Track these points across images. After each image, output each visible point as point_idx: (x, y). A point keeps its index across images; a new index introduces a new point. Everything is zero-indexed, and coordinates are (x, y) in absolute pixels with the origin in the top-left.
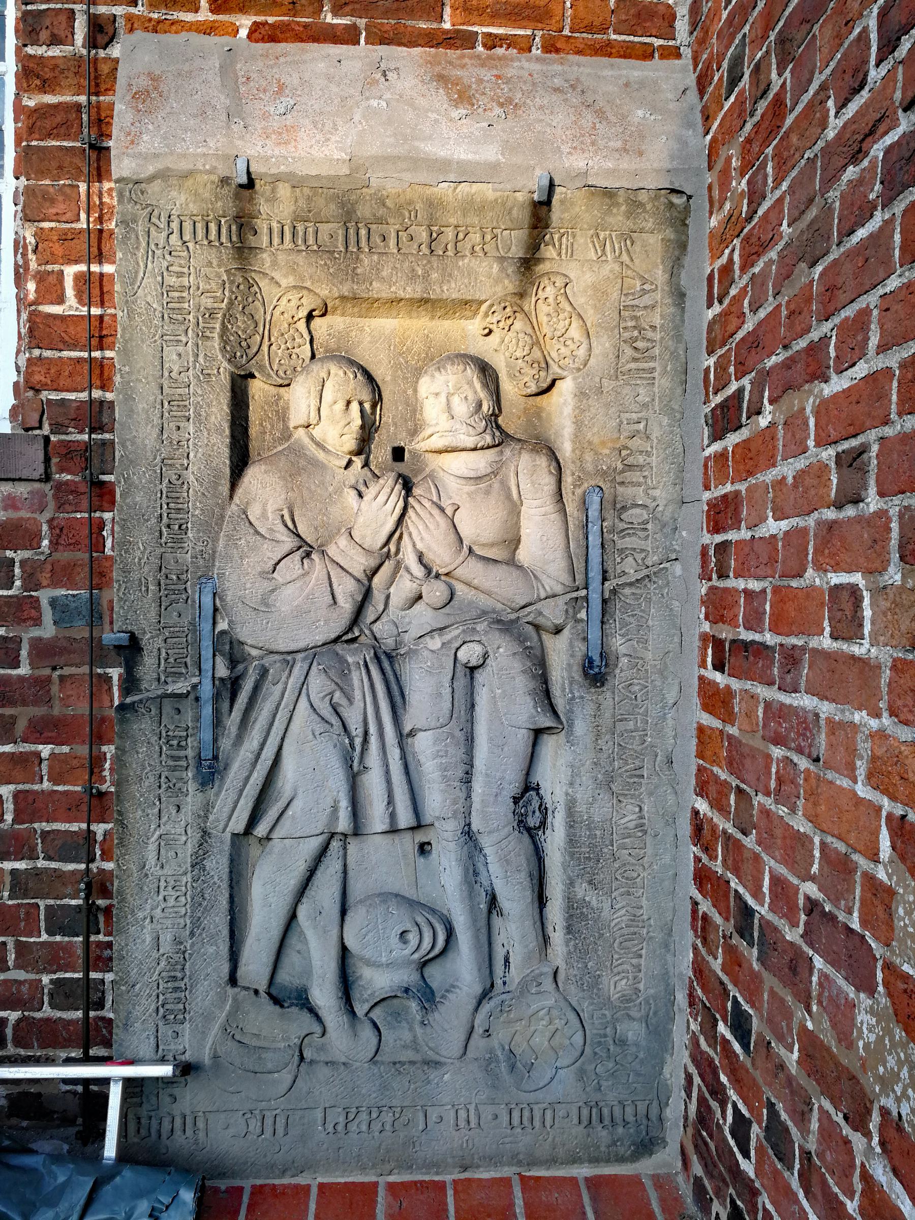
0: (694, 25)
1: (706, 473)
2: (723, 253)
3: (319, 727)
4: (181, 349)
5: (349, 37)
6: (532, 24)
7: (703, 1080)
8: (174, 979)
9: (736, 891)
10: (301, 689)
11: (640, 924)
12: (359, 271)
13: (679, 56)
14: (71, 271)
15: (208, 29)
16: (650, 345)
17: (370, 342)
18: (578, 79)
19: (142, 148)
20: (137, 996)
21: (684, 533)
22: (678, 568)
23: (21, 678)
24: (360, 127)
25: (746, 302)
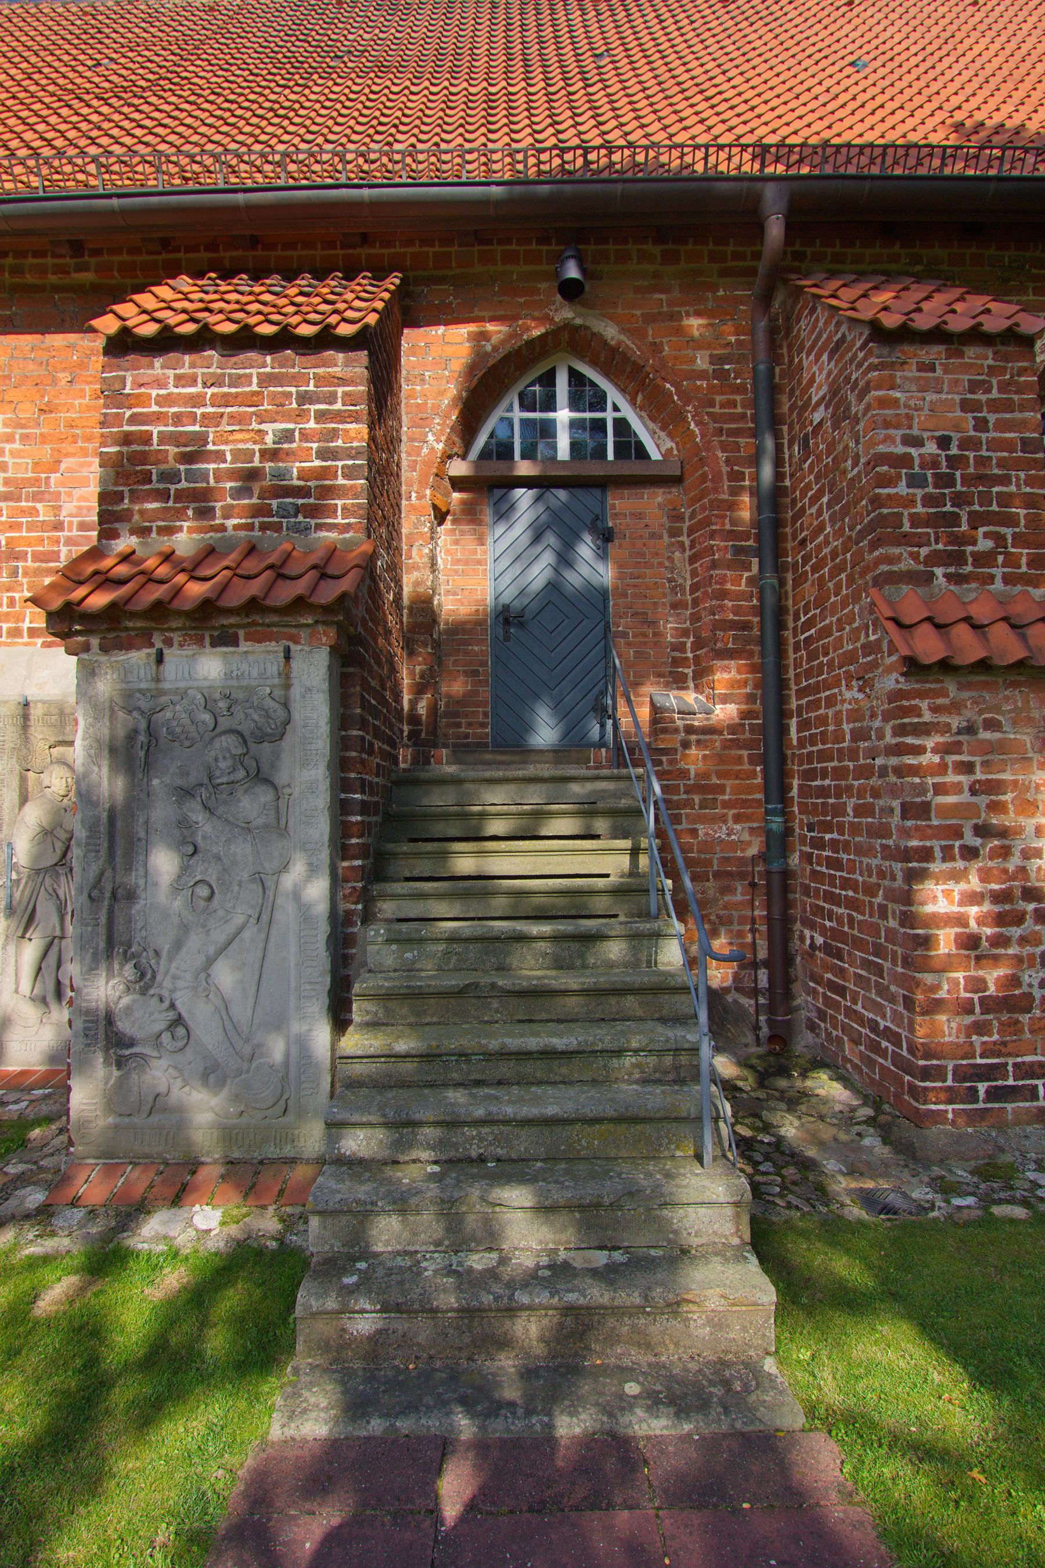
15: (26, 644)
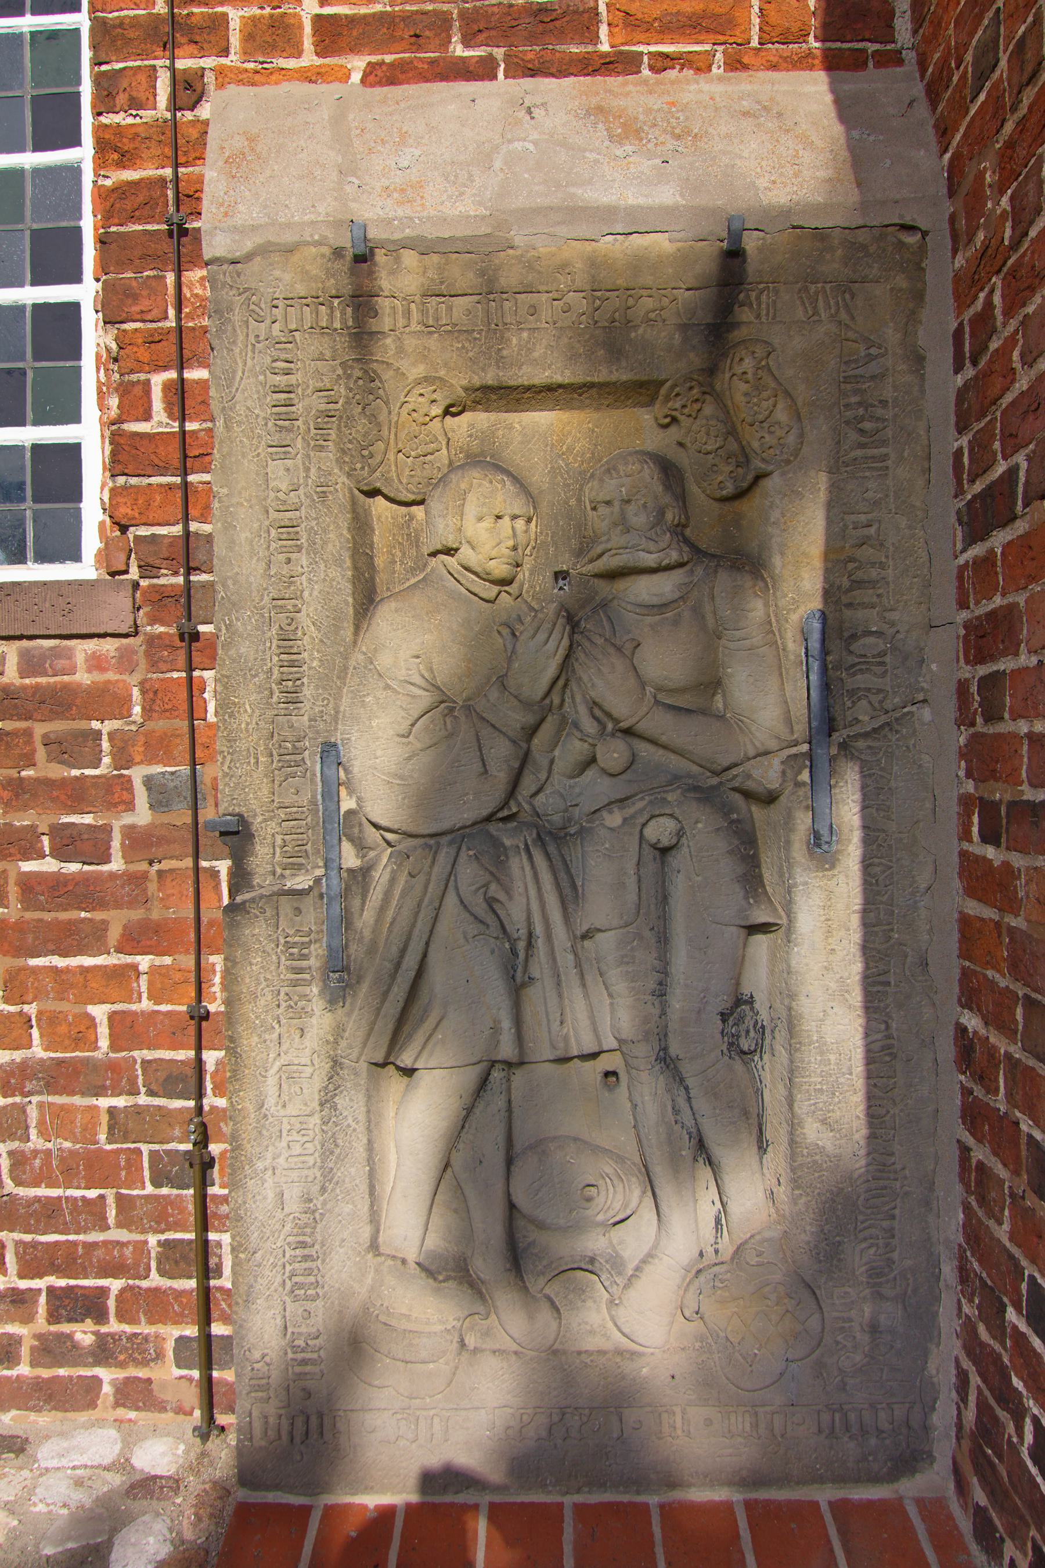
0: (918, 22)
1: (961, 587)
2: (976, 297)
3: (472, 929)
4: (289, 463)
5: (484, 71)
6: (712, 37)
7: (985, 1380)
8: (303, 1245)
9: (1030, 1136)
10: (448, 881)
11: (892, 1176)
12: (505, 353)
13: (900, 62)
14: (158, 380)
15: (310, 76)
16: (880, 425)
17: (522, 443)
18: (772, 99)
19: (239, 220)
20: (259, 1265)
21: (934, 667)
22: (926, 714)
23: (112, 876)
24: (501, 175)
25: (1016, 355)
